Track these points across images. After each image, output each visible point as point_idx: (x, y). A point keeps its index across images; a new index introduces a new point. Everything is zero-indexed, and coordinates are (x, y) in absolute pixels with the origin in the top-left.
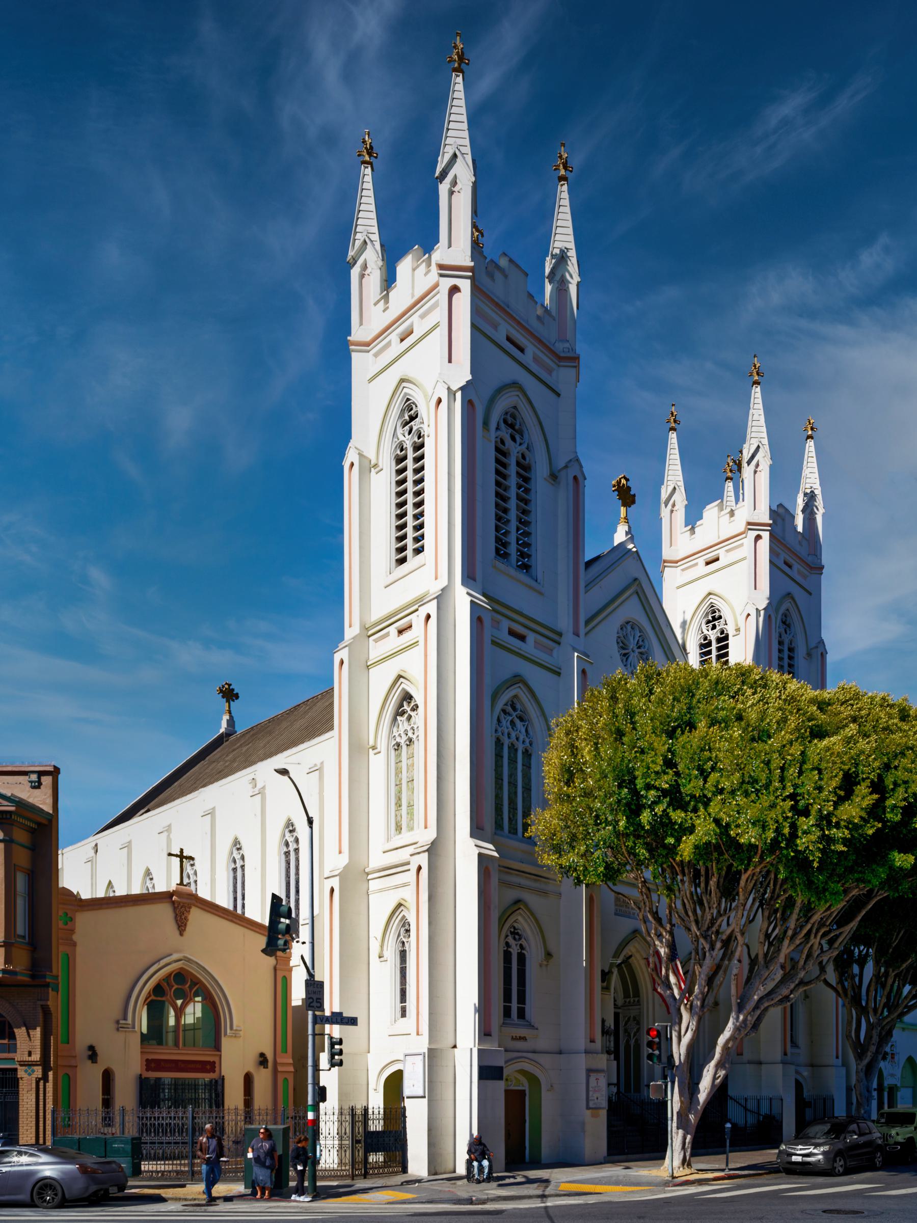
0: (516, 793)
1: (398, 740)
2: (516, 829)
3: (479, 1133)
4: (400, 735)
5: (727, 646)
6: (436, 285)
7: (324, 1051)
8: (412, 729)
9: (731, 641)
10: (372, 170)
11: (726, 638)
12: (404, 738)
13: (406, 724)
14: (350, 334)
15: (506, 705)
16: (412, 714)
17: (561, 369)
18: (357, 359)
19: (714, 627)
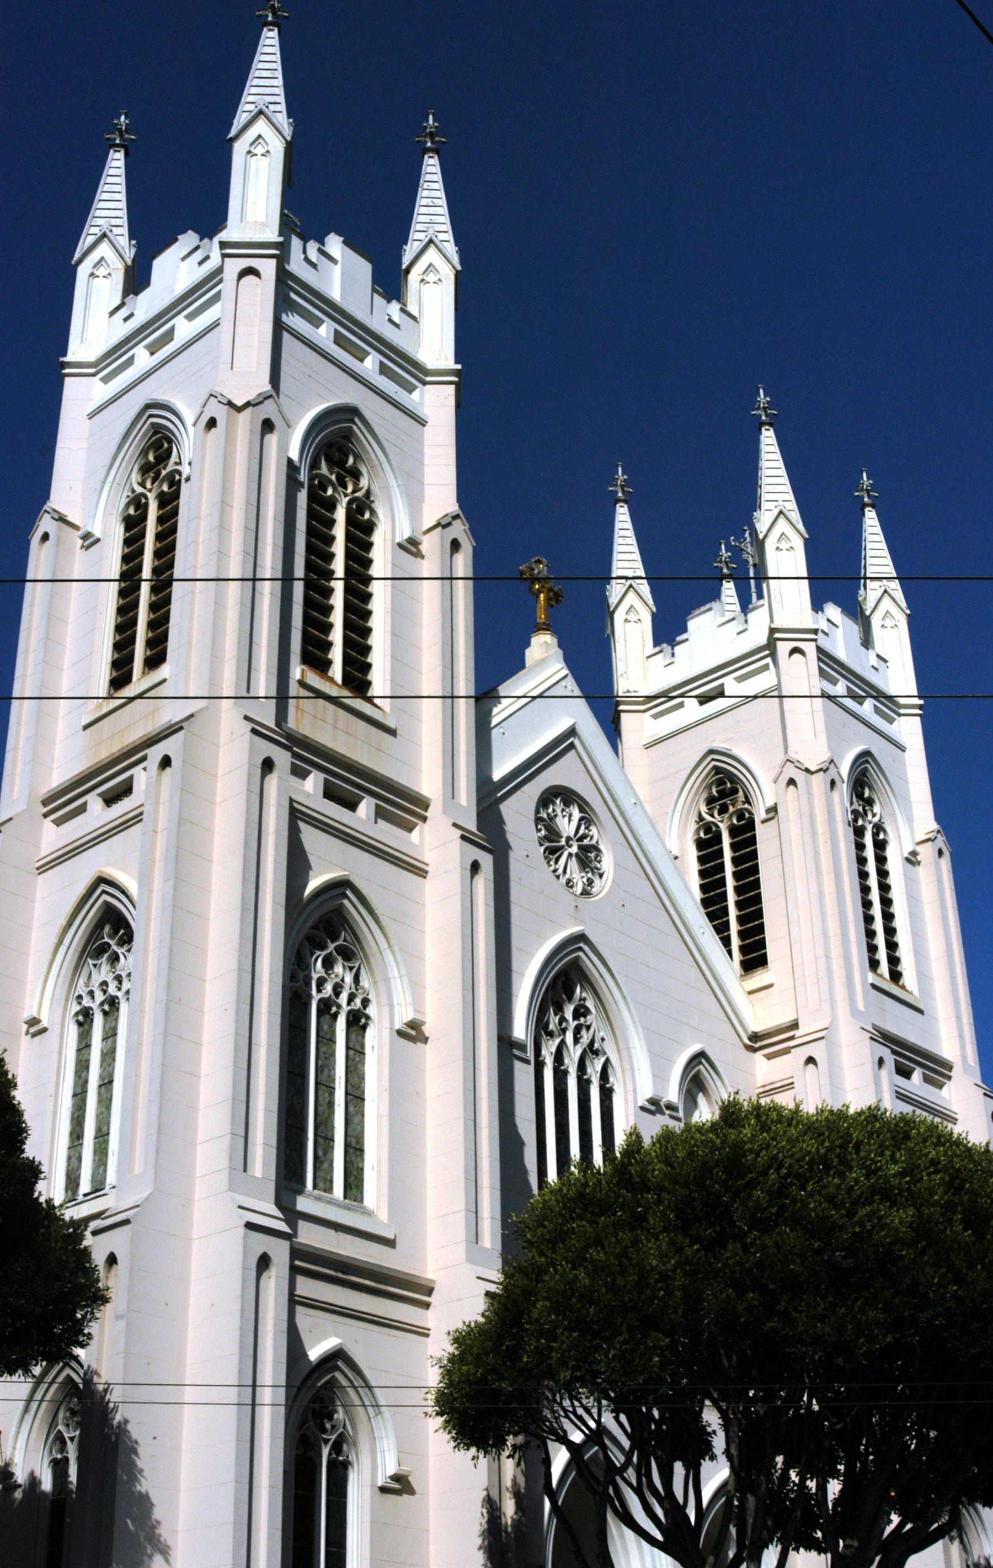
0: (331, 1105)
1: (86, 1002)
2: (331, 1182)
3: (757, 442)
4: (91, 993)
5: (753, 841)
6: (220, 270)
7: (303, 487)
8: (119, 979)
9: (760, 830)
10: (126, 155)
11: (751, 825)
12: (99, 997)
13: (105, 968)
14: (65, 355)
15: (314, 927)
16: (120, 951)
17: (428, 386)
18: (72, 388)
19: (723, 810)
